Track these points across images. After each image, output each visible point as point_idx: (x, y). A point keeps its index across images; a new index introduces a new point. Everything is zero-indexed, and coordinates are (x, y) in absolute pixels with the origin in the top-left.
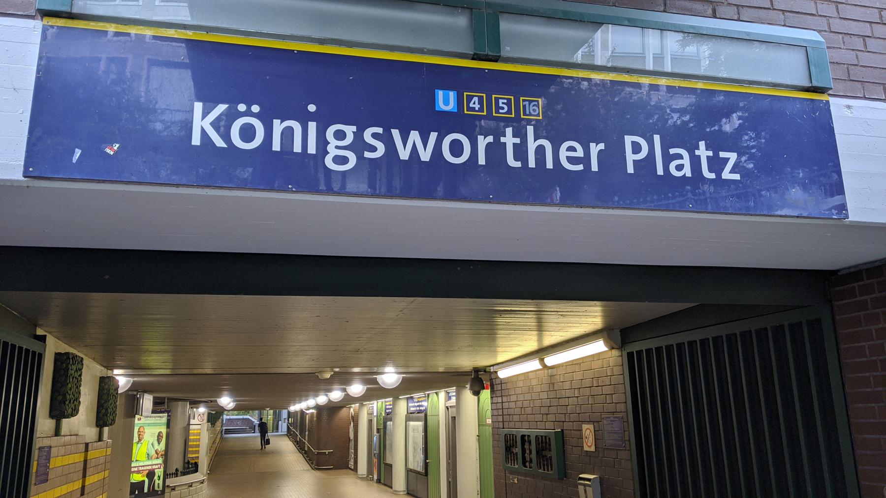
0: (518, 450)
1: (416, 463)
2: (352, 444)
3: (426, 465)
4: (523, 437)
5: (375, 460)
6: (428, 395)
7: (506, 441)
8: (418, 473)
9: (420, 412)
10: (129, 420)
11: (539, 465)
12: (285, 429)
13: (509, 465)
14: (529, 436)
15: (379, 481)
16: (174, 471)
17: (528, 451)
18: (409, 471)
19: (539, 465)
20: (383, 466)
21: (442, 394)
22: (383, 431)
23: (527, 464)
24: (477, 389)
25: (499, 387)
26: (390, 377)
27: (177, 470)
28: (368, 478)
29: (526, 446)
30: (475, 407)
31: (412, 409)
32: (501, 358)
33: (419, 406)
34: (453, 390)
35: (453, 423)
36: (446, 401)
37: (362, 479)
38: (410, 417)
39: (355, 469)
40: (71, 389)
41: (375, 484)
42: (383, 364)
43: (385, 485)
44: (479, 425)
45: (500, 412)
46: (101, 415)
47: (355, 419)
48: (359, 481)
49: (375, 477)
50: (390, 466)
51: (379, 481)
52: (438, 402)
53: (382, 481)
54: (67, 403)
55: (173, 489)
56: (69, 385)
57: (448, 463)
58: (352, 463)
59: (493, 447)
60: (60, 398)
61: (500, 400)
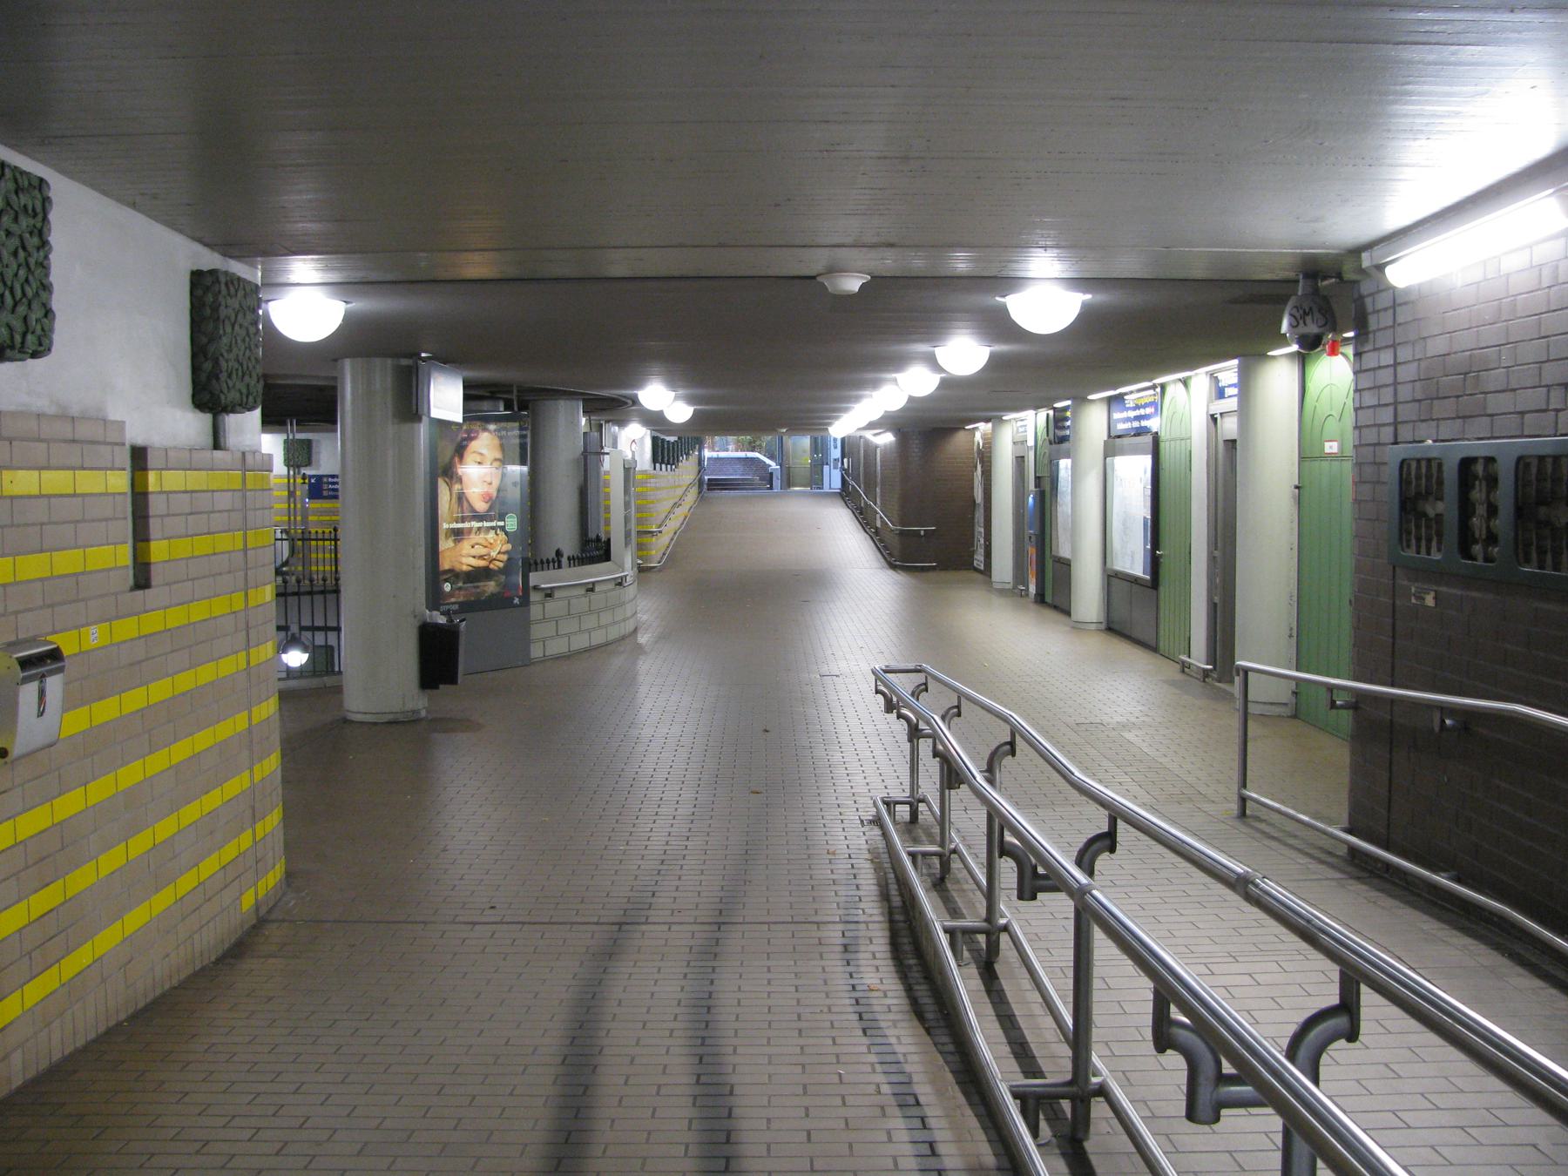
0: (1445, 508)
1: (1132, 560)
2: (979, 515)
3: (1155, 563)
4: (1466, 464)
5: (1032, 551)
6: (1163, 387)
7: (1404, 481)
8: (1134, 580)
9: (1140, 432)
10: (406, 427)
11: (1522, 551)
12: (837, 484)
13: (1411, 553)
14: (1490, 460)
15: (1041, 599)
16: (552, 555)
17: (1481, 510)
18: (1113, 579)
19: (1522, 551)
20: (1049, 564)
21: (1200, 378)
22: (1047, 488)
23: (1477, 549)
24: (1312, 329)
25: (1386, 319)
26: (1046, 300)
27: (559, 553)
28: (1015, 592)
29: (1478, 494)
30: (1303, 397)
31: (1121, 427)
32: (1394, 216)
33: (1138, 418)
34: (1228, 371)
35: (1229, 456)
36: (1210, 401)
37: (1002, 592)
38: (1114, 444)
39: (987, 571)
40: (230, 351)
41: (1033, 607)
42: (1020, 244)
43: (1056, 608)
44: (1302, 458)
45: (1387, 396)
46: (203, 377)
47: (986, 457)
48: (997, 601)
49: (1032, 589)
50: (1065, 565)
51: (1041, 599)
52: (1189, 401)
53: (1048, 599)
54: (223, 377)
55: (549, 594)
56: (225, 340)
57: (1212, 559)
58: (979, 559)
59: (1357, 501)
60: (208, 366)
61: (1386, 358)
